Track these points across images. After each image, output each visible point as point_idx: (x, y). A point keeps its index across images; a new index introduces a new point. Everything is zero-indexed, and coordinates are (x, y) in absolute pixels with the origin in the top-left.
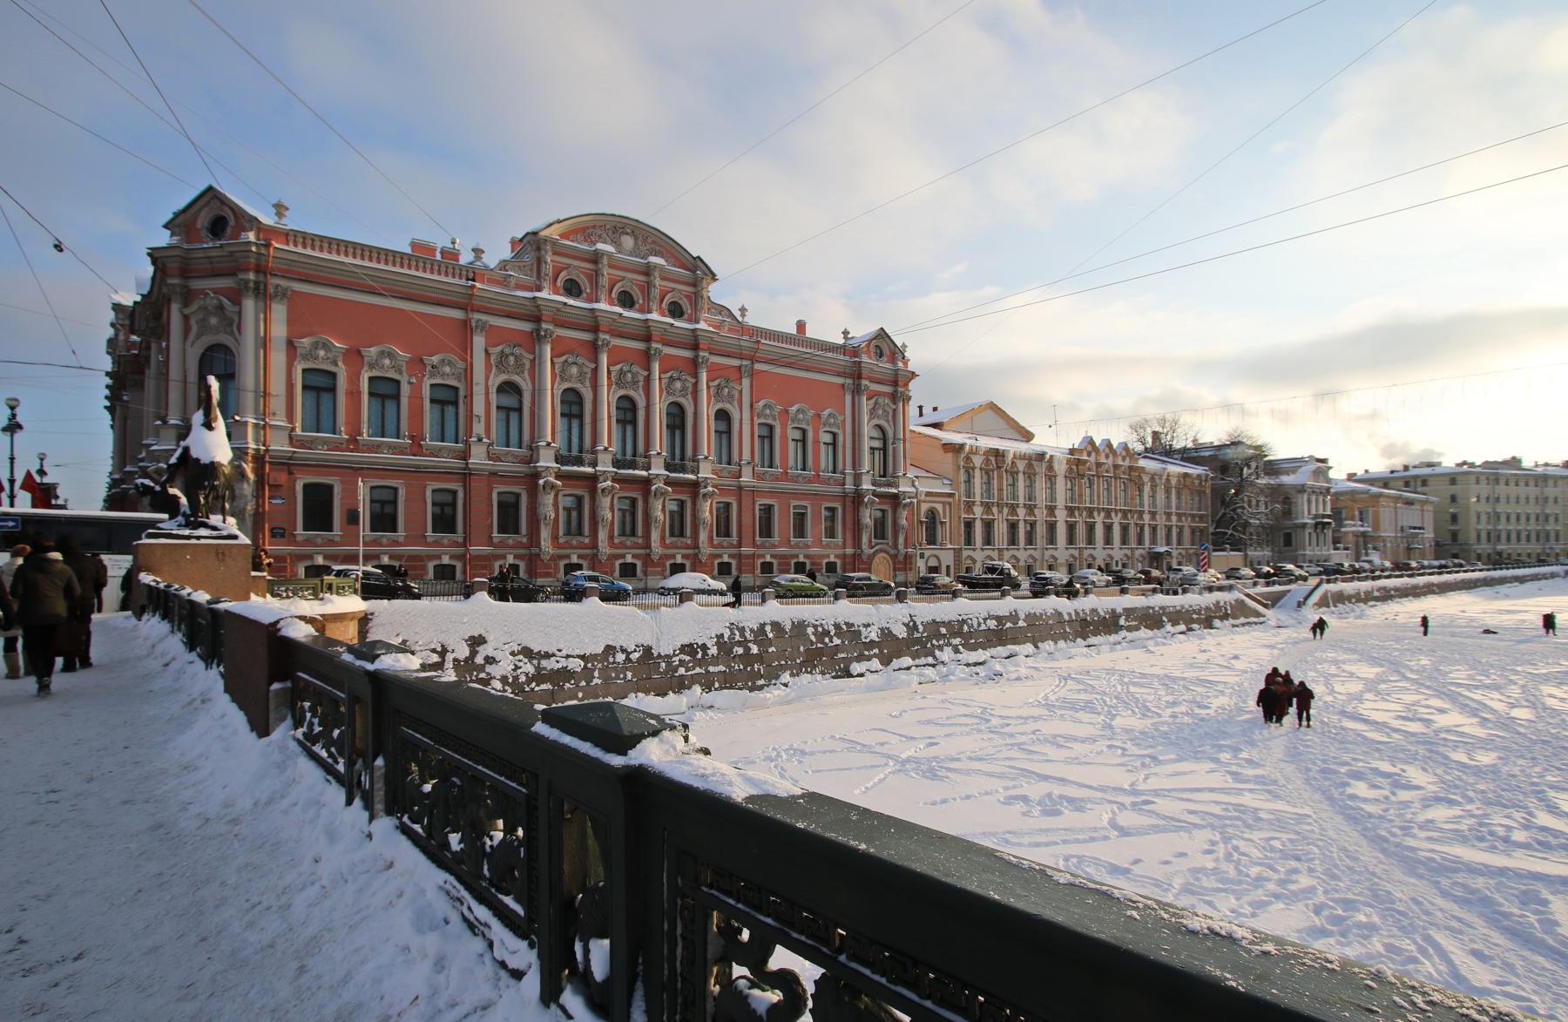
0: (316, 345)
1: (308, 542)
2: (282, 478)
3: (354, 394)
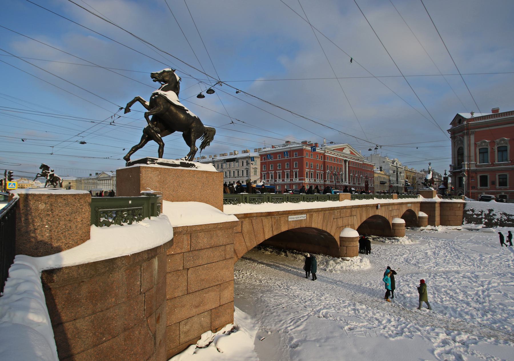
0: (482, 143)
1: (481, 189)
2: (474, 175)
3: (493, 152)
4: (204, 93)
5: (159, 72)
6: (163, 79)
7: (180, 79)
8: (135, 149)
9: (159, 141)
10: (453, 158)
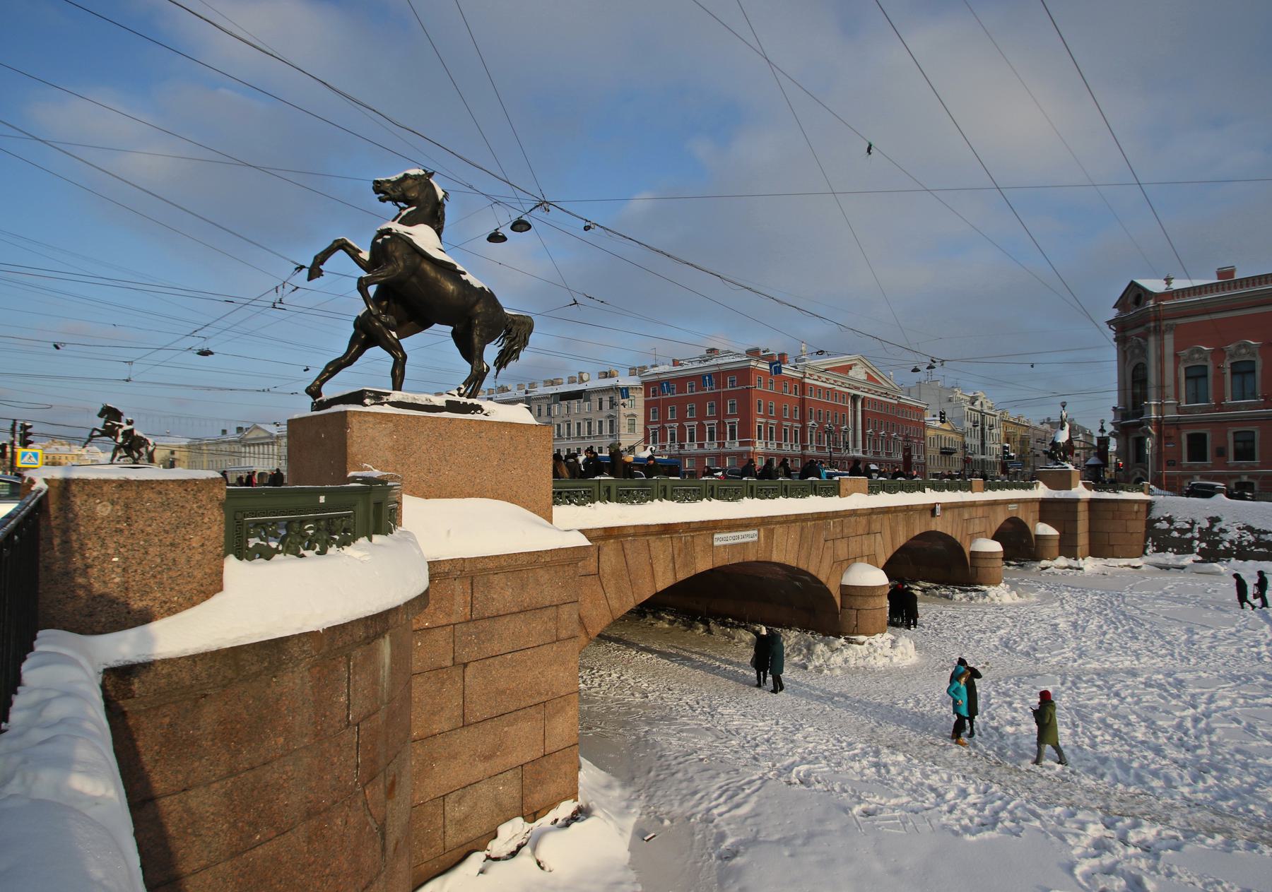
0: (1192, 353)
1: (1190, 468)
2: (1172, 432)
3: (1219, 377)
4: (506, 231)
5: (393, 178)
6: (404, 195)
7: (446, 196)
8: (335, 368)
9: (394, 348)
10: (1122, 390)
